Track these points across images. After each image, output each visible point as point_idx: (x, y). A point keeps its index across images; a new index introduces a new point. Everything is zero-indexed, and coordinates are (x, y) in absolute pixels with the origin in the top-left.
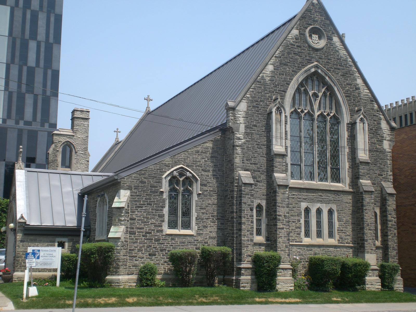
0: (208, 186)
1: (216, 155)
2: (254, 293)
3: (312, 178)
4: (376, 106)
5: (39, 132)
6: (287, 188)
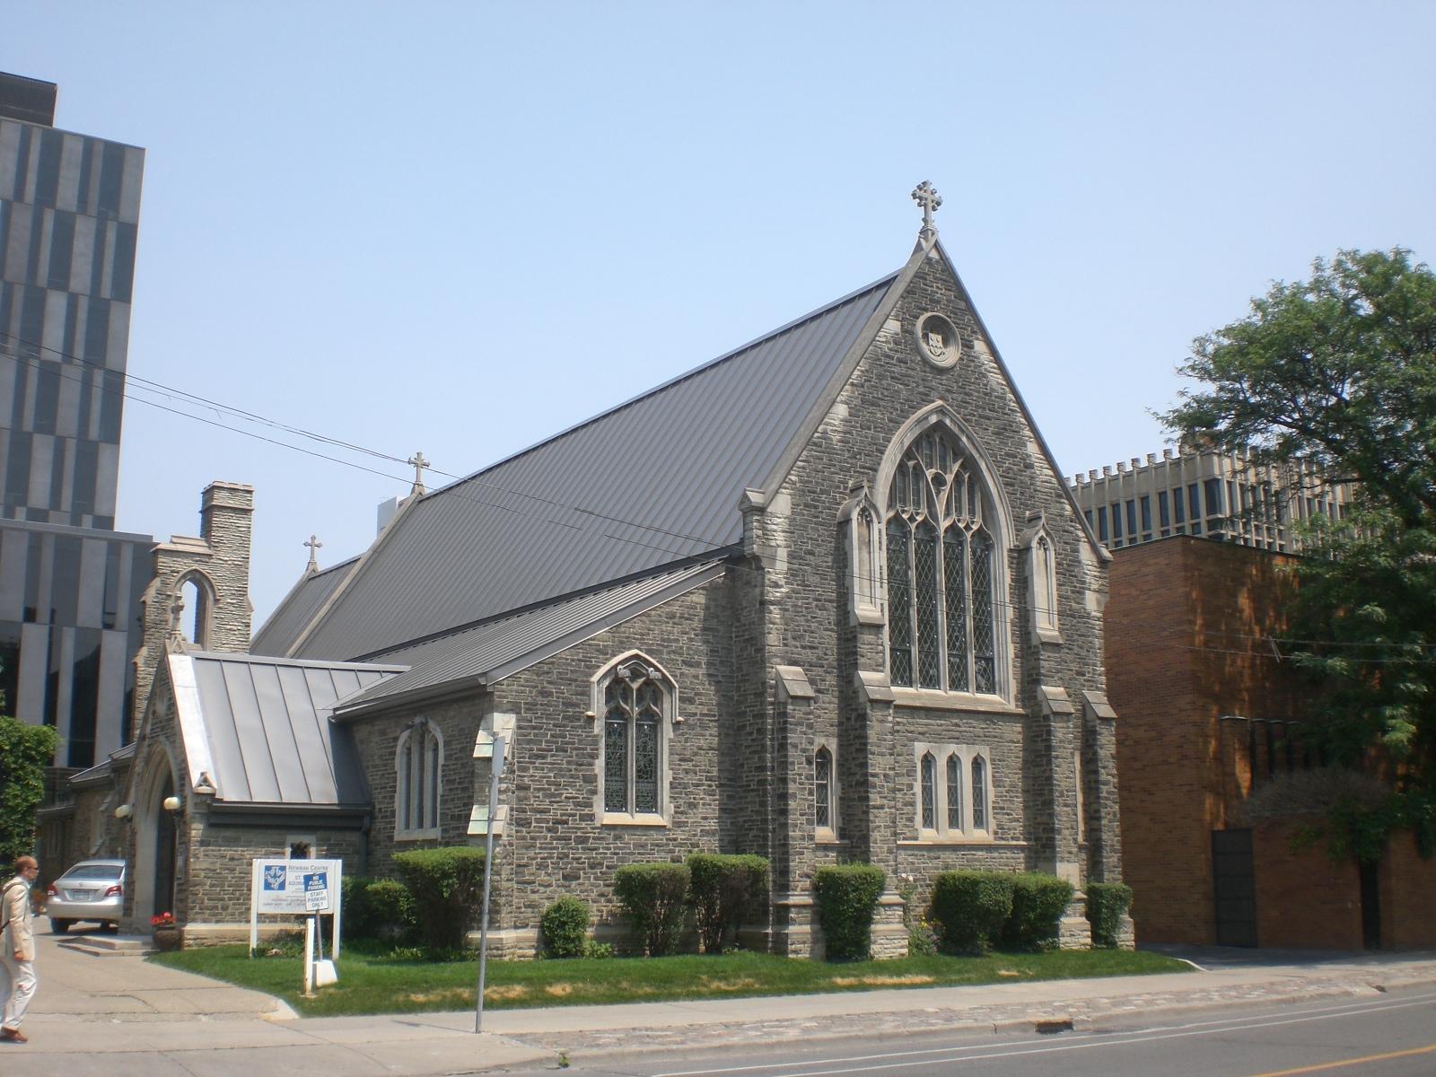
0: (697, 702)
1: (714, 623)
2: (824, 966)
3: (930, 681)
4: (1068, 507)
5: (84, 540)
6: (889, 708)
